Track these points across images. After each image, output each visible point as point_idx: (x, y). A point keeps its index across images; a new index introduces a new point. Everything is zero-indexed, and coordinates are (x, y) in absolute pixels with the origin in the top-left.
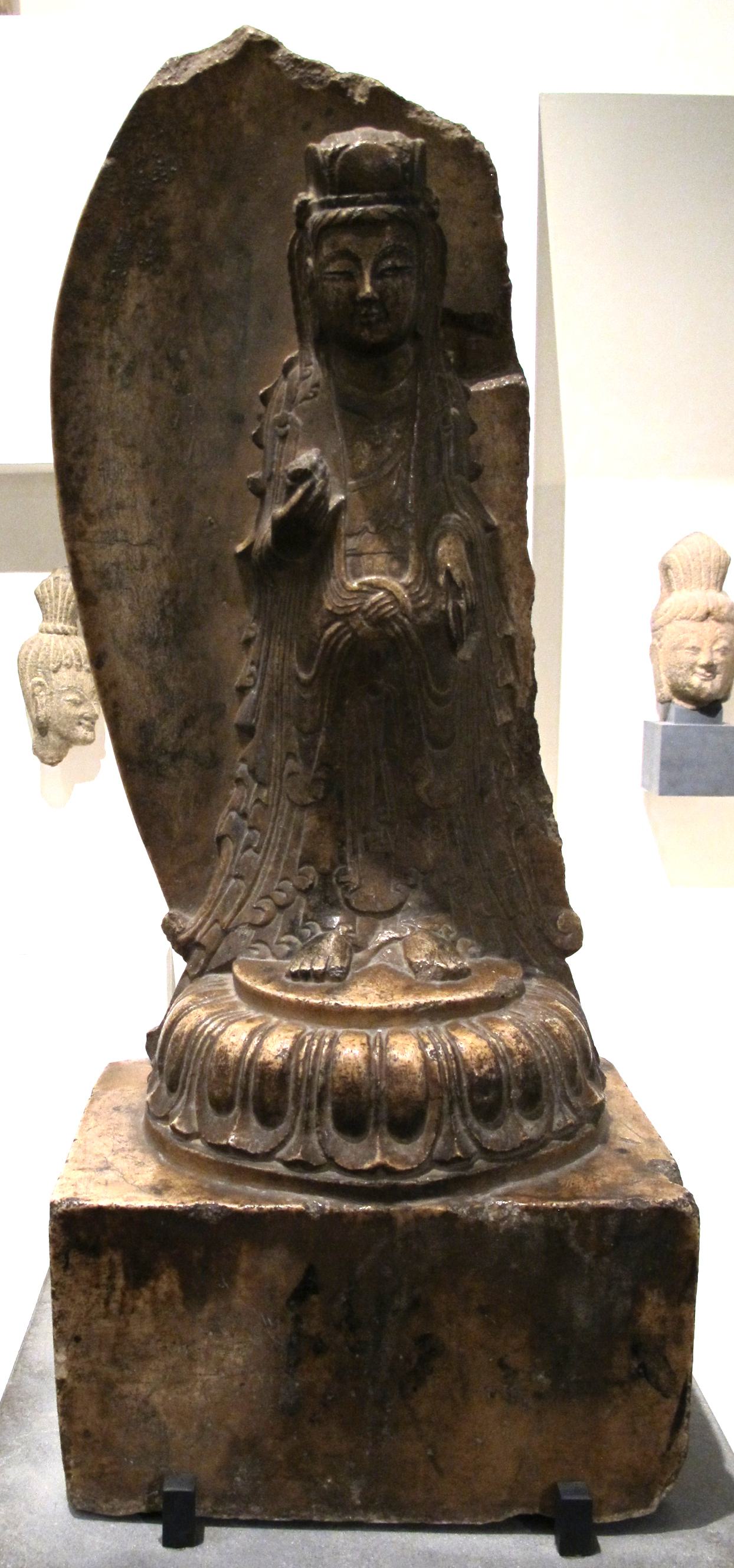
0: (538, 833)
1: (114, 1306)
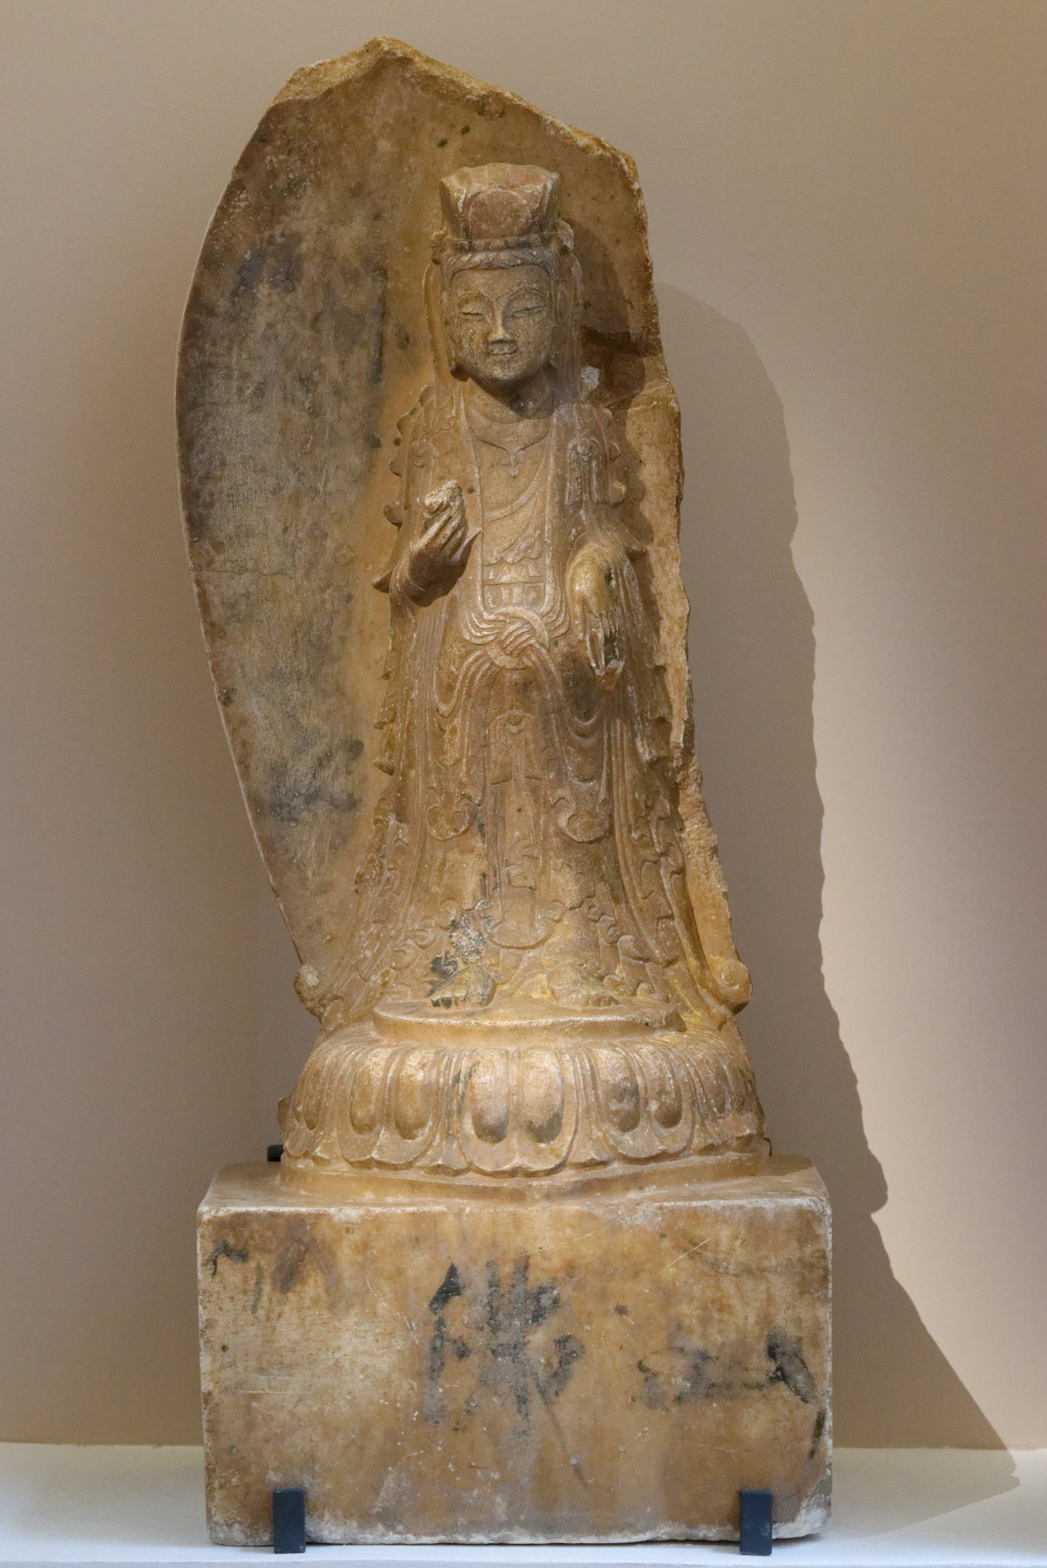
0: (699, 877)
1: (261, 1313)
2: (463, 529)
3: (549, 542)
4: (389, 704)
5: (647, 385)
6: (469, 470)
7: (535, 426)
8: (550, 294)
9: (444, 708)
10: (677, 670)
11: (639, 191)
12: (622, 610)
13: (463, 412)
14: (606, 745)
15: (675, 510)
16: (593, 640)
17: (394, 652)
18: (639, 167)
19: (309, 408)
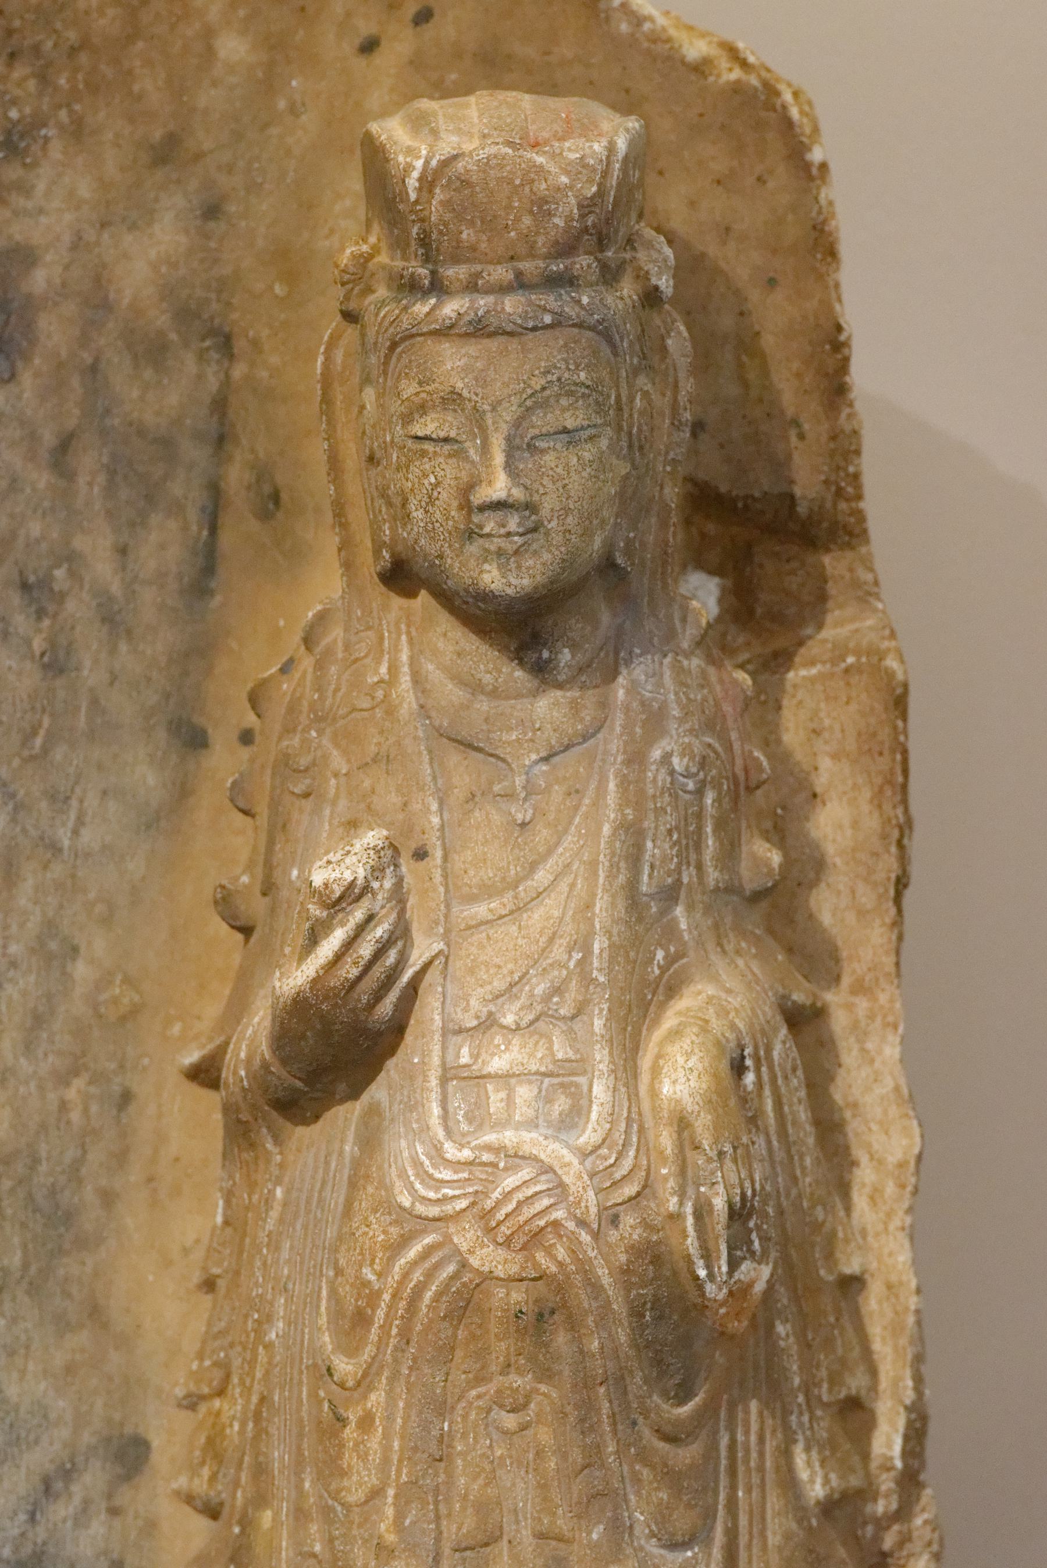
2: (400, 944)
3: (602, 979)
4: (213, 1352)
5: (829, 618)
6: (416, 806)
7: (575, 707)
8: (618, 397)
9: (345, 1367)
10: (889, 1287)
11: (824, 166)
12: (769, 1142)
13: (406, 669)
14: (724, 1462)
15: (893, 911)
16: (702, 1212)
17: (229, 1230)
18: (819, 111)
19: (43, 654)
